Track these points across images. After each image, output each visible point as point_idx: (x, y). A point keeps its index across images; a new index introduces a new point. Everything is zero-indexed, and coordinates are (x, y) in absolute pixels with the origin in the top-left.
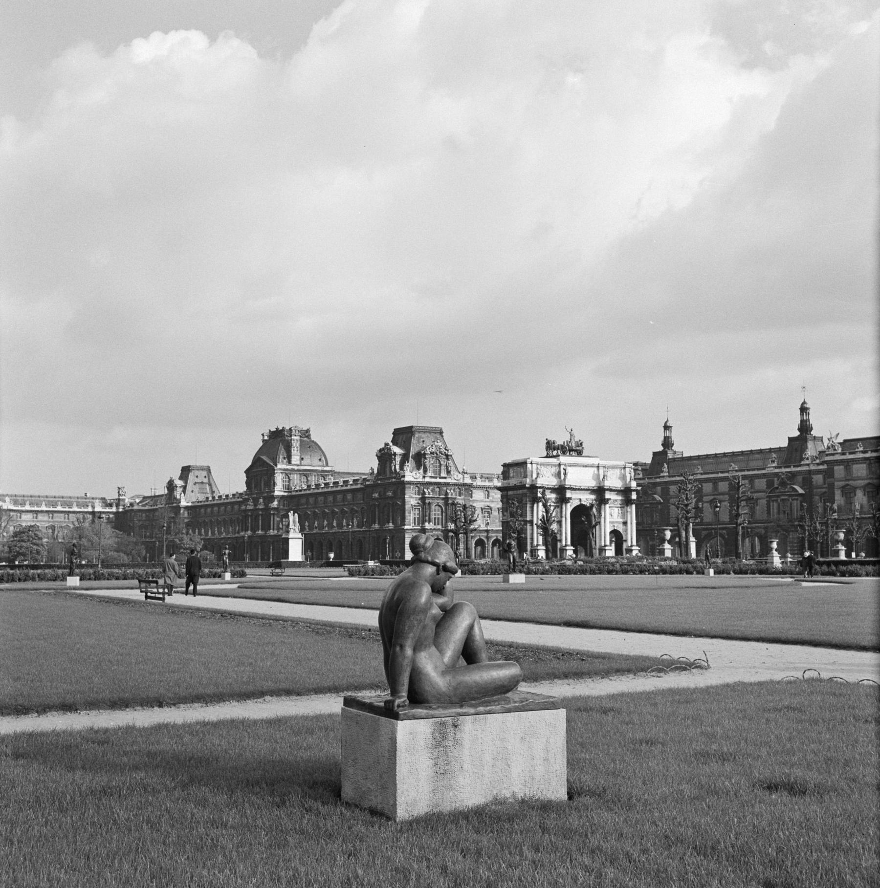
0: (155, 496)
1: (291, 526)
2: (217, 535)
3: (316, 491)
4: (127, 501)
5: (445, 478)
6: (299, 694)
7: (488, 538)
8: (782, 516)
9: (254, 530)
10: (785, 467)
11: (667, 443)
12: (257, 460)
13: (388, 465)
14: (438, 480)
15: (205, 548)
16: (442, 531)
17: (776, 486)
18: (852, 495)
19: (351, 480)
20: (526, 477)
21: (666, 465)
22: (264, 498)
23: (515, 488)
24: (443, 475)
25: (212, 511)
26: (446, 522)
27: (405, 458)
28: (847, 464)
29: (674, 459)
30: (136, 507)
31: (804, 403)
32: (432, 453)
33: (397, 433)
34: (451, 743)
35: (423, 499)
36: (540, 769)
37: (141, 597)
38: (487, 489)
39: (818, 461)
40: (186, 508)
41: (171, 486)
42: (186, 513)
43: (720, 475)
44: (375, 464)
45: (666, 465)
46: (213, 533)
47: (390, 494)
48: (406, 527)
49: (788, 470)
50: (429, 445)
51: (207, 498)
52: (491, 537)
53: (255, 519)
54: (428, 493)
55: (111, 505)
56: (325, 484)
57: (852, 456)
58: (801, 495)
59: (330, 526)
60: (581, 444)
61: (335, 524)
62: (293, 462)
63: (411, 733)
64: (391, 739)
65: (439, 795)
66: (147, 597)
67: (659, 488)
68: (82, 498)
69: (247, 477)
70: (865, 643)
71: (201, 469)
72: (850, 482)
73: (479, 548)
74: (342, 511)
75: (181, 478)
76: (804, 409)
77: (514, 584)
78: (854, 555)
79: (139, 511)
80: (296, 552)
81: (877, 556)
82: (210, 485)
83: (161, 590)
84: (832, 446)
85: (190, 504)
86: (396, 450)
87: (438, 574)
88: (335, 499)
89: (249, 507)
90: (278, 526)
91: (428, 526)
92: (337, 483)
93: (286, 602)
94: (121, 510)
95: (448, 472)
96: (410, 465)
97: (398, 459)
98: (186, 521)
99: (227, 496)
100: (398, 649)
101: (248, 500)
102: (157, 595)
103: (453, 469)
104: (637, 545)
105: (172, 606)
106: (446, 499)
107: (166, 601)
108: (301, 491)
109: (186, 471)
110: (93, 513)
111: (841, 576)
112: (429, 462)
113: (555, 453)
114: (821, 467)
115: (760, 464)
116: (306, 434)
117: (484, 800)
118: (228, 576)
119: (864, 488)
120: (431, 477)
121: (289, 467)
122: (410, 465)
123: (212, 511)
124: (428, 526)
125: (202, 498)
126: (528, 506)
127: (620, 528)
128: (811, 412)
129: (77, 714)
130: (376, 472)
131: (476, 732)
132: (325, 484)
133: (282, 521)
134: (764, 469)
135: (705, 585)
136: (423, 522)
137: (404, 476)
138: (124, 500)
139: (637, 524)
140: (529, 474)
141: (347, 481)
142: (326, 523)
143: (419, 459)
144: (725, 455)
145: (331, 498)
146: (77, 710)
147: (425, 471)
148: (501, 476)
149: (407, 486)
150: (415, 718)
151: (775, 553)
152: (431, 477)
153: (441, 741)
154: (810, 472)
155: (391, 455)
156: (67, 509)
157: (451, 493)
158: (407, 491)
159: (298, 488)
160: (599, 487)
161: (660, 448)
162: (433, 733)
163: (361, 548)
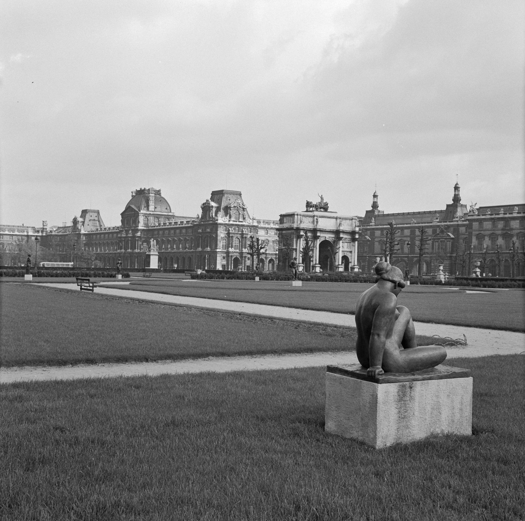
0: (65, 227)
1: (152, 248)
2: (103, 252)
3: (164, 227)
4: (48, 230)
5: (242, 222)
6: (229, 356)
7: (266, 258)
8: (440, 250)
9: (126, 249)
10: (444, 222)
11: (375, 206)
12: (128, 208)
13: (208, 212)
14: (238, 223)
15: (96, 259)
16: (239, 253)
17: (438, 233)
18: (496, 239)
19: (185, 221)
20: (293, 223)
21: (373, 219)
22: (132, 230)
23: (287, 229)
24: (241, 220)
25: (100, 237)
26: (242, 248)
27: (218, 209)
28: (481, 221)
29: (379, 215)
30: (53, 233)
31: (457, 184)
32: (235, 207)
33: (214, 194)
34: (408, 399)
35: (229, 234)
36: (458, 416)
37: (78, 288)
38: (266, 229)
39: (463, 219)
40: (84, 234)
41: (75, 221)
42: (84, 237)
43: (405, 225)
44: (200, 212)
45: (373, 219)
46: (101, 250)
47: (208, 230)
48: (218, 250)
49: (446, 224)
50: (232, 201)
51: (97, 229)
52: (268, 258)
53: (127, 243)
54: (231, 230)
55: (38, 232)
56: (169, 223)
57: (483, 217)
58: (452, 238)
59: (172, 248)
60: (327, 204)
61: (175, 247)
62: (150, 210)
63: (386, 392)
64: (372, 395)
65: (401, 432)
66: (81, 289)
67: (369, 232)
68: (21, 227)
69: (122, 217)
70: (518, 327)
71: (94, 211)
72: (482, 232)
73: (270, 265)
74: (179, 239)
75: (81, 217)
76: (456, 188)
77: (295, 287)
78: (484, 275)
79: (56, 235)
80: (154, 263)
81: (523, 275)
82: (99, 221)
83: (91, 285)
84: (473, 210)
85: (87, 232)
86: (213, 204)
87: (395, 288)
88: (175, 233)
89: (123, 235)
90: (140, 247)
91: (231, 250)
92: (177, 222)
93: (169, 294)
94: (44, 235)
95: (244, 218)
96: (221, 213)
97: (214, 210)
98: (84, 242)
99: (109, 228)
100: (376, 337)
101: (122, 231)
102: (88, 288)
103: (246, 217)
104: (303, 263)
105: (98, 294)
106: (242, 234)
107: (94, 291)
108: (154, 227)
109: (84, 213)
110: (28, 236)
111: (483, 287)
112: (233, 212)
113: (311, 209)
114: (465, 223)
115: (429, 220)
116: (158, 192)
117: (426, 435)
118: (120, 277)
119: (517, 234)
120: (234, 221)
121: (148, 212)
122: (221, 213)
123: (100, 237)
124: (231, 250)
125: (94, 229)
126: (295, 240)
127: (348, 255)
128: (460, 189)
129: (96, 366)
130: (200, 217)
131: (422, 392)
132: (169, 223)
133: (143, 244)
134: (431, 223)
135: (418, 291)
136: (228, 248)
137: (217, 220)
138: (46, 229)
139: (358, 252)
140: (296, 221)
141: (183, 222)
142: (169, 246)
143: (227, 210)
144: (409, 214)
145: (172, 232)
146: (96, 363)
147: (230, 217)
148: (279, 222)
149: (219, 226)
150: (388, 382)
151: (441, 272)
152: (234, 221)
153: (402, 397)
154: (458, 225)
155: (210, 207)
156: (11, 233)
157: (245, 231)
158: (219, 229)
159: (153, 225)
160: (337, 230)
161: (371, 209)
162: (398, 392)
163: (190, 262)
